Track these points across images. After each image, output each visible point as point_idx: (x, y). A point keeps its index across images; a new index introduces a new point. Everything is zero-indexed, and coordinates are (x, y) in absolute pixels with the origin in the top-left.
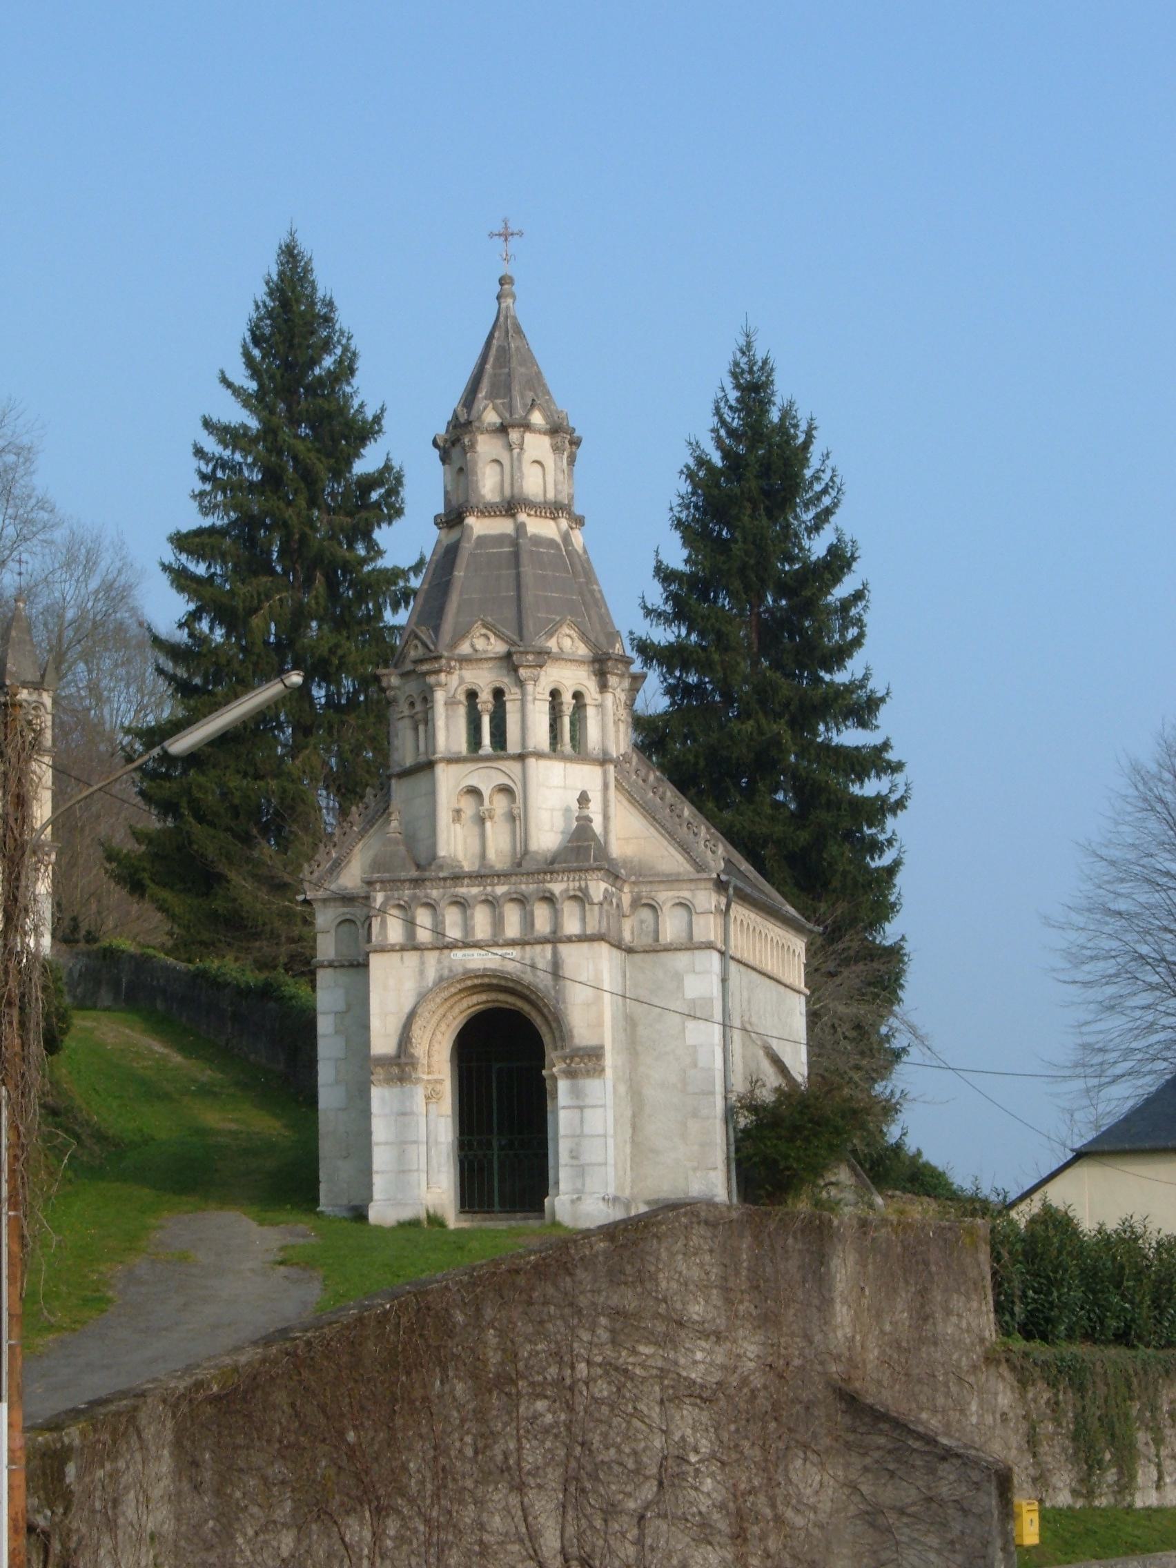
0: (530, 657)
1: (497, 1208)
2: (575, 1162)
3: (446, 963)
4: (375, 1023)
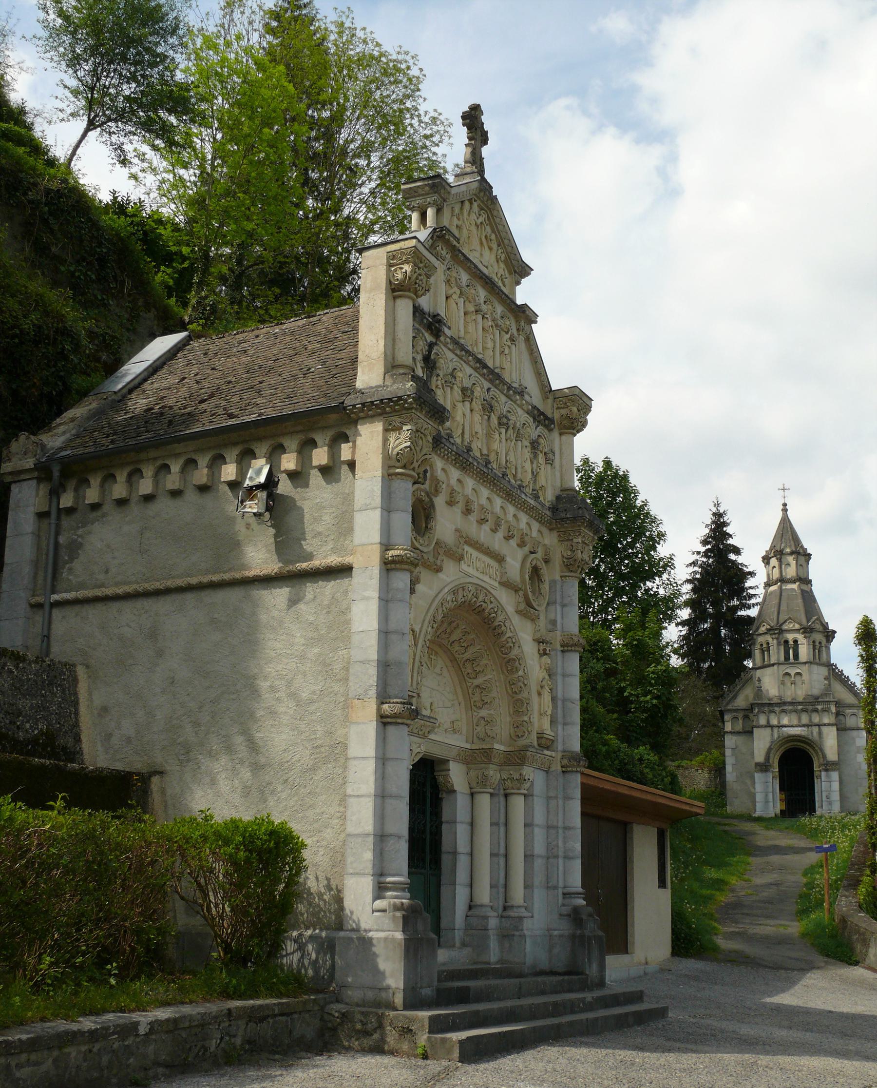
4: (756, 751)
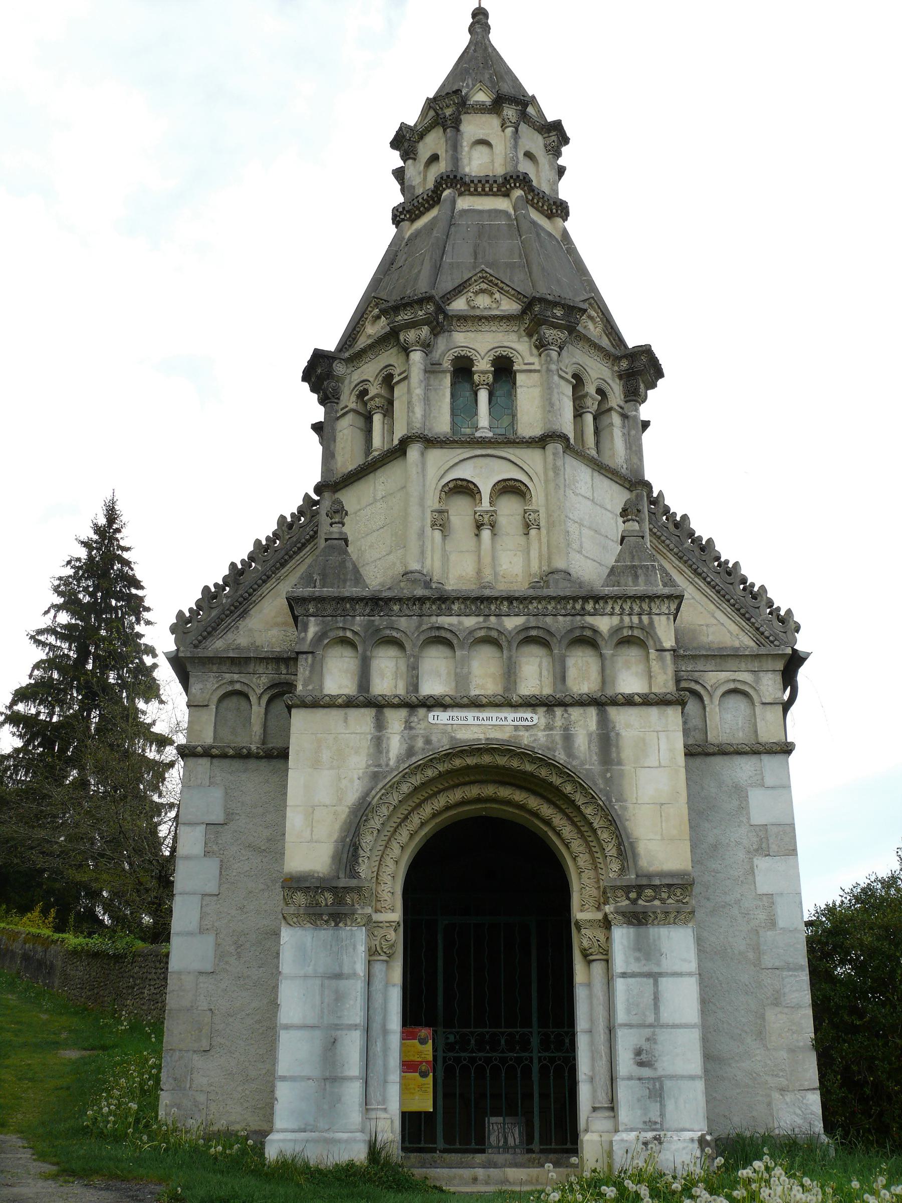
0: (559, 312)
1: (441, 1144)
2: (646, 1072)
3: (420, 729)
4: (295, 820)
